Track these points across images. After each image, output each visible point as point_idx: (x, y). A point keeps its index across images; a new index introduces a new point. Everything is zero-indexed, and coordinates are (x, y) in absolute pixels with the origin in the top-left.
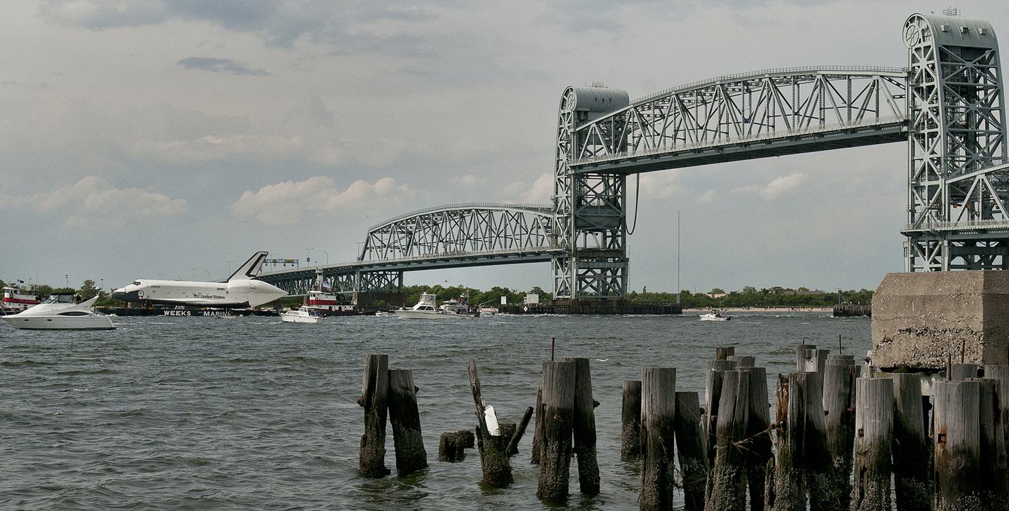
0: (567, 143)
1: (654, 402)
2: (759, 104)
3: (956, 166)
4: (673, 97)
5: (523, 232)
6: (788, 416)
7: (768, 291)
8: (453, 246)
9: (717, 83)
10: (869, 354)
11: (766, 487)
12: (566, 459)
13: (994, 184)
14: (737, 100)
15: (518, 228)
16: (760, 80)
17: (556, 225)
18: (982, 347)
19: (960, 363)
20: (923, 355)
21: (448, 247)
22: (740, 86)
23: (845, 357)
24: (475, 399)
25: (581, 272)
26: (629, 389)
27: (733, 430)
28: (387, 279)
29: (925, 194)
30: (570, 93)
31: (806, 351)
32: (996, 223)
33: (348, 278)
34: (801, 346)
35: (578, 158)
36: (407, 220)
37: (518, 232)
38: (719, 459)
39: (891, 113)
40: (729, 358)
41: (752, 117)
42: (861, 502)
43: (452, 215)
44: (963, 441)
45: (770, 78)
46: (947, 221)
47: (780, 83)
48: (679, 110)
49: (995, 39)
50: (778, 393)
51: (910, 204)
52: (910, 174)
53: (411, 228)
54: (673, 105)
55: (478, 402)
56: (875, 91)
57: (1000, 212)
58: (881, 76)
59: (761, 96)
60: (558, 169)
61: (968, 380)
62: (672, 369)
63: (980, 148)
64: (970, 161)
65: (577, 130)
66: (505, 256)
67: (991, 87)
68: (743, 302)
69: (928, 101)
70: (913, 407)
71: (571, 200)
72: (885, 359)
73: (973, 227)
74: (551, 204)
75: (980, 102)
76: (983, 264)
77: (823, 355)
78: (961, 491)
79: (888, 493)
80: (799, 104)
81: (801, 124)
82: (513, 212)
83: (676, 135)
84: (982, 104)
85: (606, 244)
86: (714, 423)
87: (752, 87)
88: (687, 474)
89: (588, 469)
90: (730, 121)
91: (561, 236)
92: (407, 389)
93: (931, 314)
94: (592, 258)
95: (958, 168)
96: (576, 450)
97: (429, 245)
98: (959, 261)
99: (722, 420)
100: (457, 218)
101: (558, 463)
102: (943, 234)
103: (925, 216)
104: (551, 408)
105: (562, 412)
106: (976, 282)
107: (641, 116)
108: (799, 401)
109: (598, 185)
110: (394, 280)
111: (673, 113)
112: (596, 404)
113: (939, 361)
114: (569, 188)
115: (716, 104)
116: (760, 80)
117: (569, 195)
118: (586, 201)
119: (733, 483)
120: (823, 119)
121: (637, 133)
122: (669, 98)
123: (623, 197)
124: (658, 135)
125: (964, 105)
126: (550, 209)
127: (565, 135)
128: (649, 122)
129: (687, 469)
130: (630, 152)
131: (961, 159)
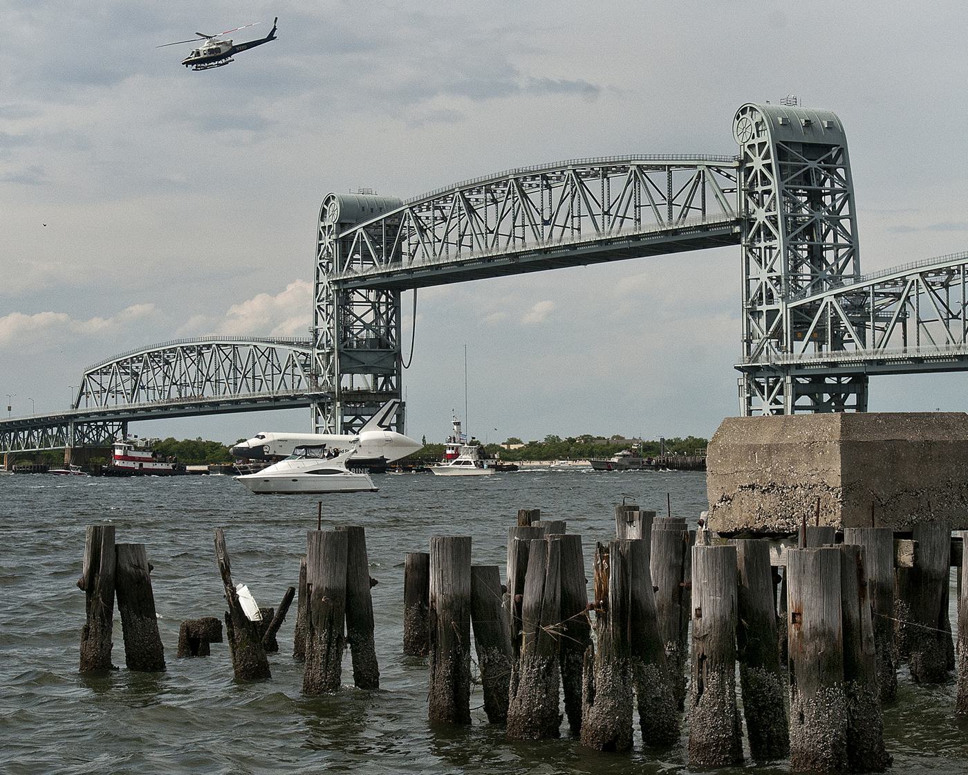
0: (328, 263)
1: (446, 578)
2: (562, 202)
3: (800, 287)
4: (456, 194)
5: (276, 371)
6: (610, 594)
7: (574, 440)
8: (189, 389)
9: (510, 177)
10: (703, 515)
11: (584, 681)
12: (337, 651)
13: (845, 308)
14: (535, 197)
15: (269, 367)
16: (562, 172)
17: (316, 362)
18: (840, 506)
19: (815, 525)
20: (770, 517)
21: (183, 391)
22: (538, 181)
23: (675, 520)
24: (224, 579)
25: (348, 419)
26: (412, 564)
27: (542, 612)
28: (108, 432)
29: (763, 322)
30: (332, 201)
31: (627, 514)
32: (848, 355)
33: (60, 431)
34: (620, 508)
35: (341, 270)
36: (132, 358)
37: (269, 371)
38: (526, 648)
39: (720, 211)
40: (535, 524)
41: (553, 218)
42: (699, 697)
43: (188, 352)
44: (823, 620)
45: (574, 170)
46: (789, 353)
47: (585, 176)
48: (465, 211)
49: (843, 133)
50: (597, 567)
51: (745, 332)
52: (745, 300)
53: (137, 368)
54: (457, 205)
55: (227, 582)
56: (700, 185)
57: (853, 341)
58: (707, 166)
59: (563, 194)
60: (317, 294)
61: (826, 546)
62: (466, 538)
63: (827, 264)
64: (816, 280)
65: (340, 236)
66: (254, 401)
67: (839, 191)
68: (545, 454)
69: (765, 208)
70: (761, 581)
71: (334, 332)
72: (724, 523)
73: (821, 360)
74: (309, 337)
75: (827, 209)
76: (833, 404)
77: (648, 518)
78: (822, 682)
79: (733, 685)
80: (609, 202)
81: (613, 224)
82: (263, 346)
83: (461, 241)
84: (828, 211)
85: (377, 384)
86: (519, 604)
87: (552, 182)
88: (486, 667)
89: (364, 662)
90: (527, 222)
91: (322, 376)
92: (139, 567)
93: (778, 467)
94: (361, 403)
95: (802, 288)
96: (349, 640)
97: (160, 388)
98: (805, 400)
99: (529, 599)
100: (194, 355)
101: (327, 656)
102: (786, 368)
103: (763, 348)
104: (318, 589)
105: (332, 593)
106: (832, 428)
107: (417, 218)
108: (622, 576)
109: (367, 313)
110: (117, 432)
111: (457, 214)
112: (374, 583)
113: (788, 524)
114: (332, 317)
115: (510, 203)
116: (562, 172)
117: (332, 326)
118: (352, 333)
119: (543, 677)
120: (639, 220)
121: (414, 239)
122: (452, 196)
123: (398, 327)
124: (440, 241)
125: (808, 213)
126: (308, 343)
127: (325, 252)
128: (428, 226)
129: (486, 662)
130: (405, 263)
131: (805, 278)
